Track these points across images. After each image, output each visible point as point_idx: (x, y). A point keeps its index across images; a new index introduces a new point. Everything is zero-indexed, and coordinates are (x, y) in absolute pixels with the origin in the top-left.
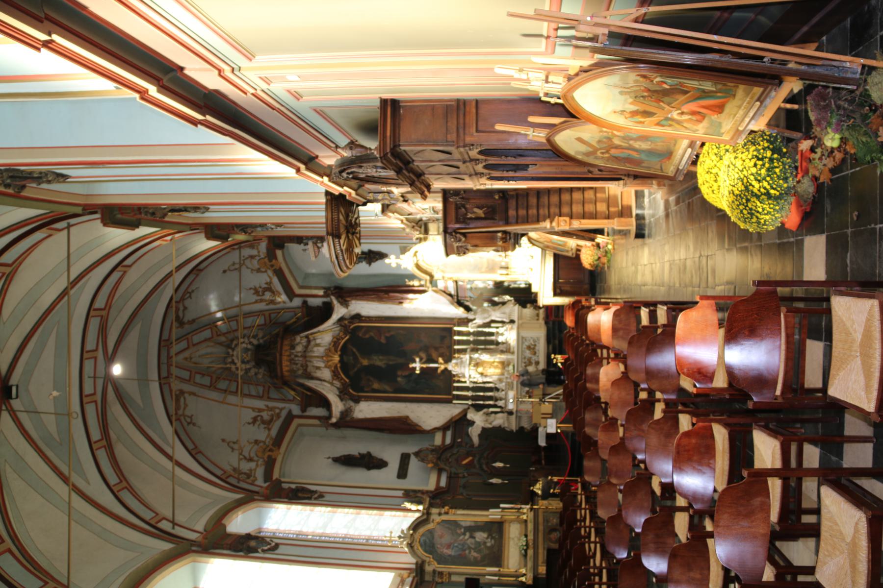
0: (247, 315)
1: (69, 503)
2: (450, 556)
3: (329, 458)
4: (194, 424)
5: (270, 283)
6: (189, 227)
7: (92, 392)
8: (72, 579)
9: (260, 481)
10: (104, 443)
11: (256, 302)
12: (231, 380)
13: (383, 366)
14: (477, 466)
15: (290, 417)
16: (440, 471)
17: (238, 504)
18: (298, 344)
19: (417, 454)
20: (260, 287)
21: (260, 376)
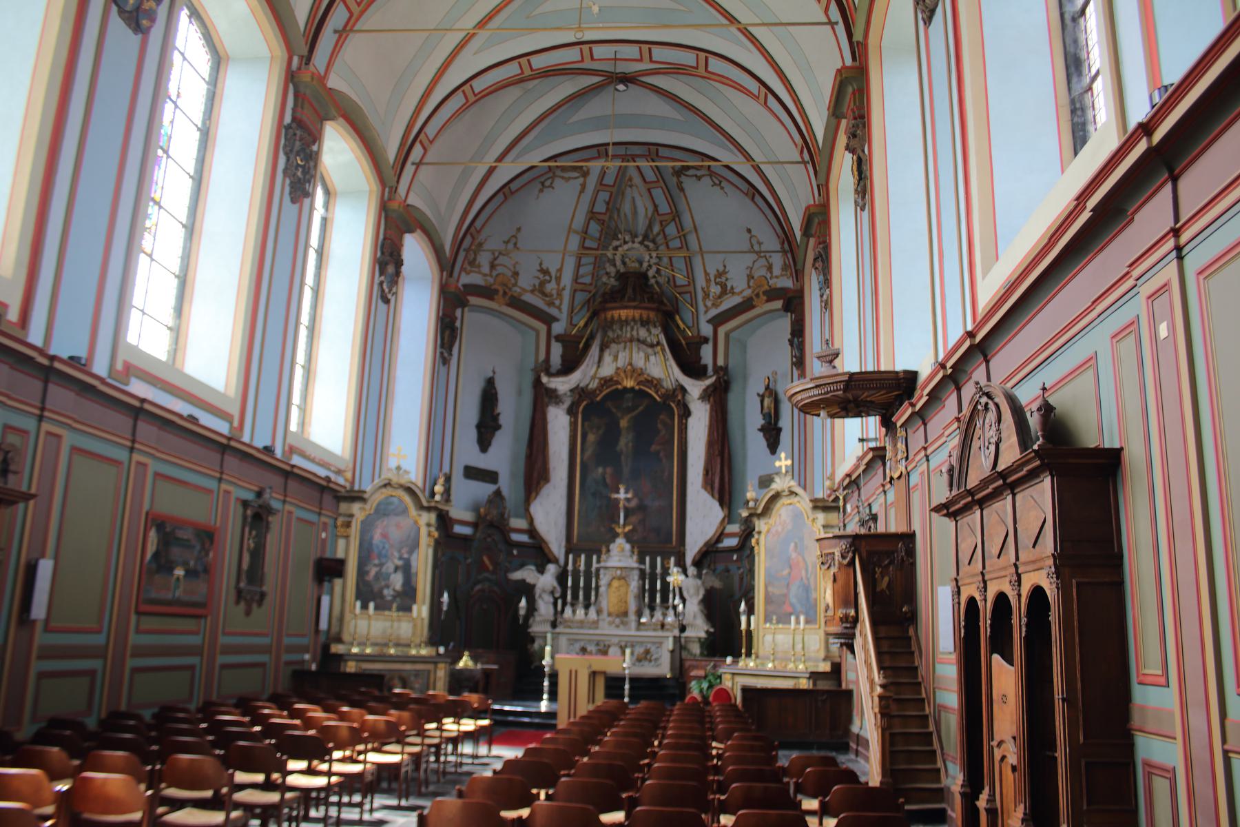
0: (689, 261)
1: (450, 30)
2: (372, 538)
3: (494, 373)
4: (541, 191)
5: (733, 293)
6: (824, 183)
7: (596, 57)
8: (358, 35)
9: (465, 279)
10: (528, 72)
11: (706, 274)
12: (600, 240)
13: (618, 448)
14: (480, 577)
15: (548, 320)
16: (475, 525)
17: (437, 250)
18: (648, 330)
19: (498, 493)
20: (727, 280)
21: (604, 279)
